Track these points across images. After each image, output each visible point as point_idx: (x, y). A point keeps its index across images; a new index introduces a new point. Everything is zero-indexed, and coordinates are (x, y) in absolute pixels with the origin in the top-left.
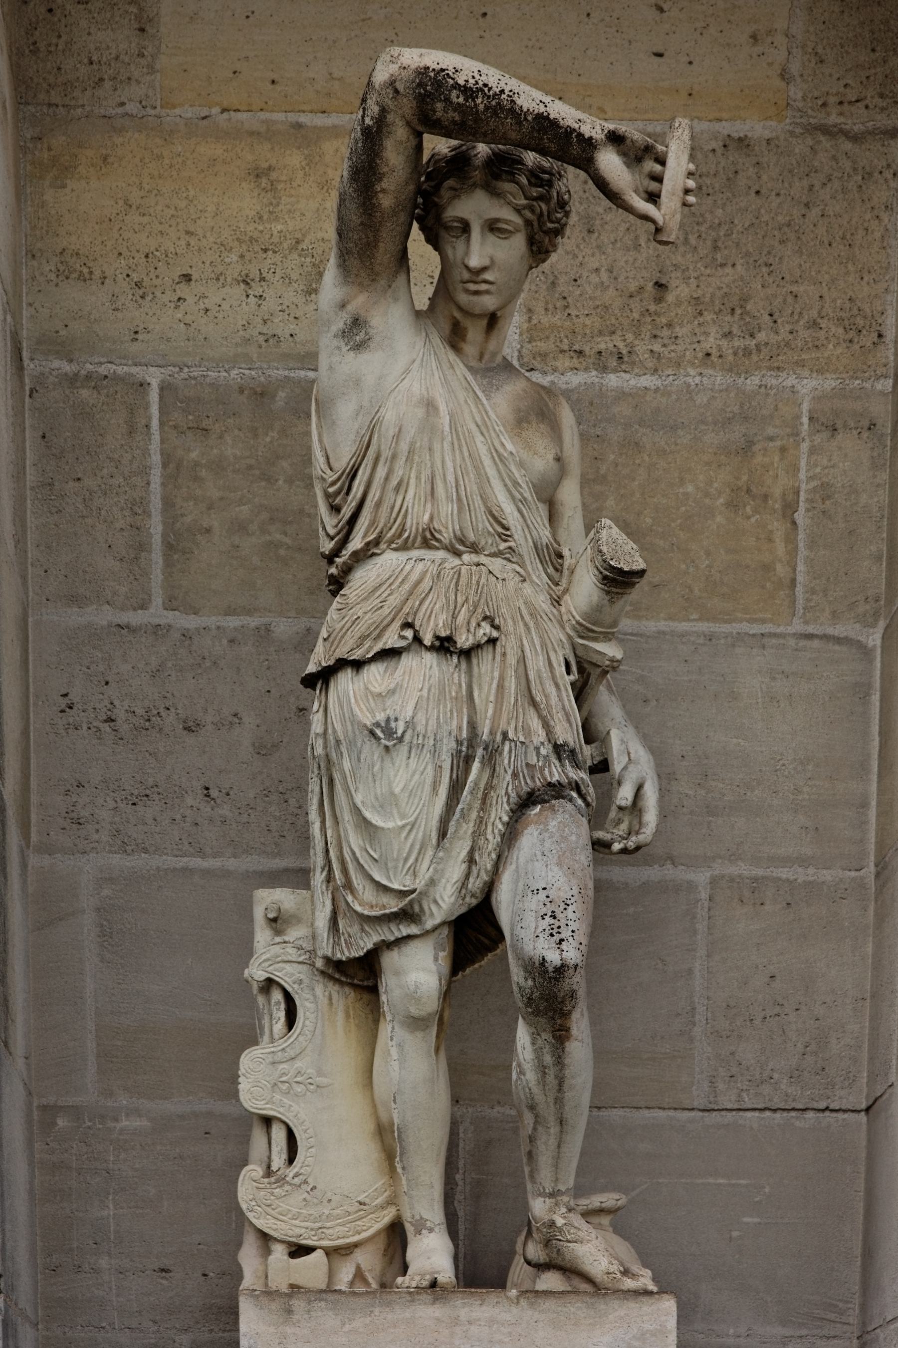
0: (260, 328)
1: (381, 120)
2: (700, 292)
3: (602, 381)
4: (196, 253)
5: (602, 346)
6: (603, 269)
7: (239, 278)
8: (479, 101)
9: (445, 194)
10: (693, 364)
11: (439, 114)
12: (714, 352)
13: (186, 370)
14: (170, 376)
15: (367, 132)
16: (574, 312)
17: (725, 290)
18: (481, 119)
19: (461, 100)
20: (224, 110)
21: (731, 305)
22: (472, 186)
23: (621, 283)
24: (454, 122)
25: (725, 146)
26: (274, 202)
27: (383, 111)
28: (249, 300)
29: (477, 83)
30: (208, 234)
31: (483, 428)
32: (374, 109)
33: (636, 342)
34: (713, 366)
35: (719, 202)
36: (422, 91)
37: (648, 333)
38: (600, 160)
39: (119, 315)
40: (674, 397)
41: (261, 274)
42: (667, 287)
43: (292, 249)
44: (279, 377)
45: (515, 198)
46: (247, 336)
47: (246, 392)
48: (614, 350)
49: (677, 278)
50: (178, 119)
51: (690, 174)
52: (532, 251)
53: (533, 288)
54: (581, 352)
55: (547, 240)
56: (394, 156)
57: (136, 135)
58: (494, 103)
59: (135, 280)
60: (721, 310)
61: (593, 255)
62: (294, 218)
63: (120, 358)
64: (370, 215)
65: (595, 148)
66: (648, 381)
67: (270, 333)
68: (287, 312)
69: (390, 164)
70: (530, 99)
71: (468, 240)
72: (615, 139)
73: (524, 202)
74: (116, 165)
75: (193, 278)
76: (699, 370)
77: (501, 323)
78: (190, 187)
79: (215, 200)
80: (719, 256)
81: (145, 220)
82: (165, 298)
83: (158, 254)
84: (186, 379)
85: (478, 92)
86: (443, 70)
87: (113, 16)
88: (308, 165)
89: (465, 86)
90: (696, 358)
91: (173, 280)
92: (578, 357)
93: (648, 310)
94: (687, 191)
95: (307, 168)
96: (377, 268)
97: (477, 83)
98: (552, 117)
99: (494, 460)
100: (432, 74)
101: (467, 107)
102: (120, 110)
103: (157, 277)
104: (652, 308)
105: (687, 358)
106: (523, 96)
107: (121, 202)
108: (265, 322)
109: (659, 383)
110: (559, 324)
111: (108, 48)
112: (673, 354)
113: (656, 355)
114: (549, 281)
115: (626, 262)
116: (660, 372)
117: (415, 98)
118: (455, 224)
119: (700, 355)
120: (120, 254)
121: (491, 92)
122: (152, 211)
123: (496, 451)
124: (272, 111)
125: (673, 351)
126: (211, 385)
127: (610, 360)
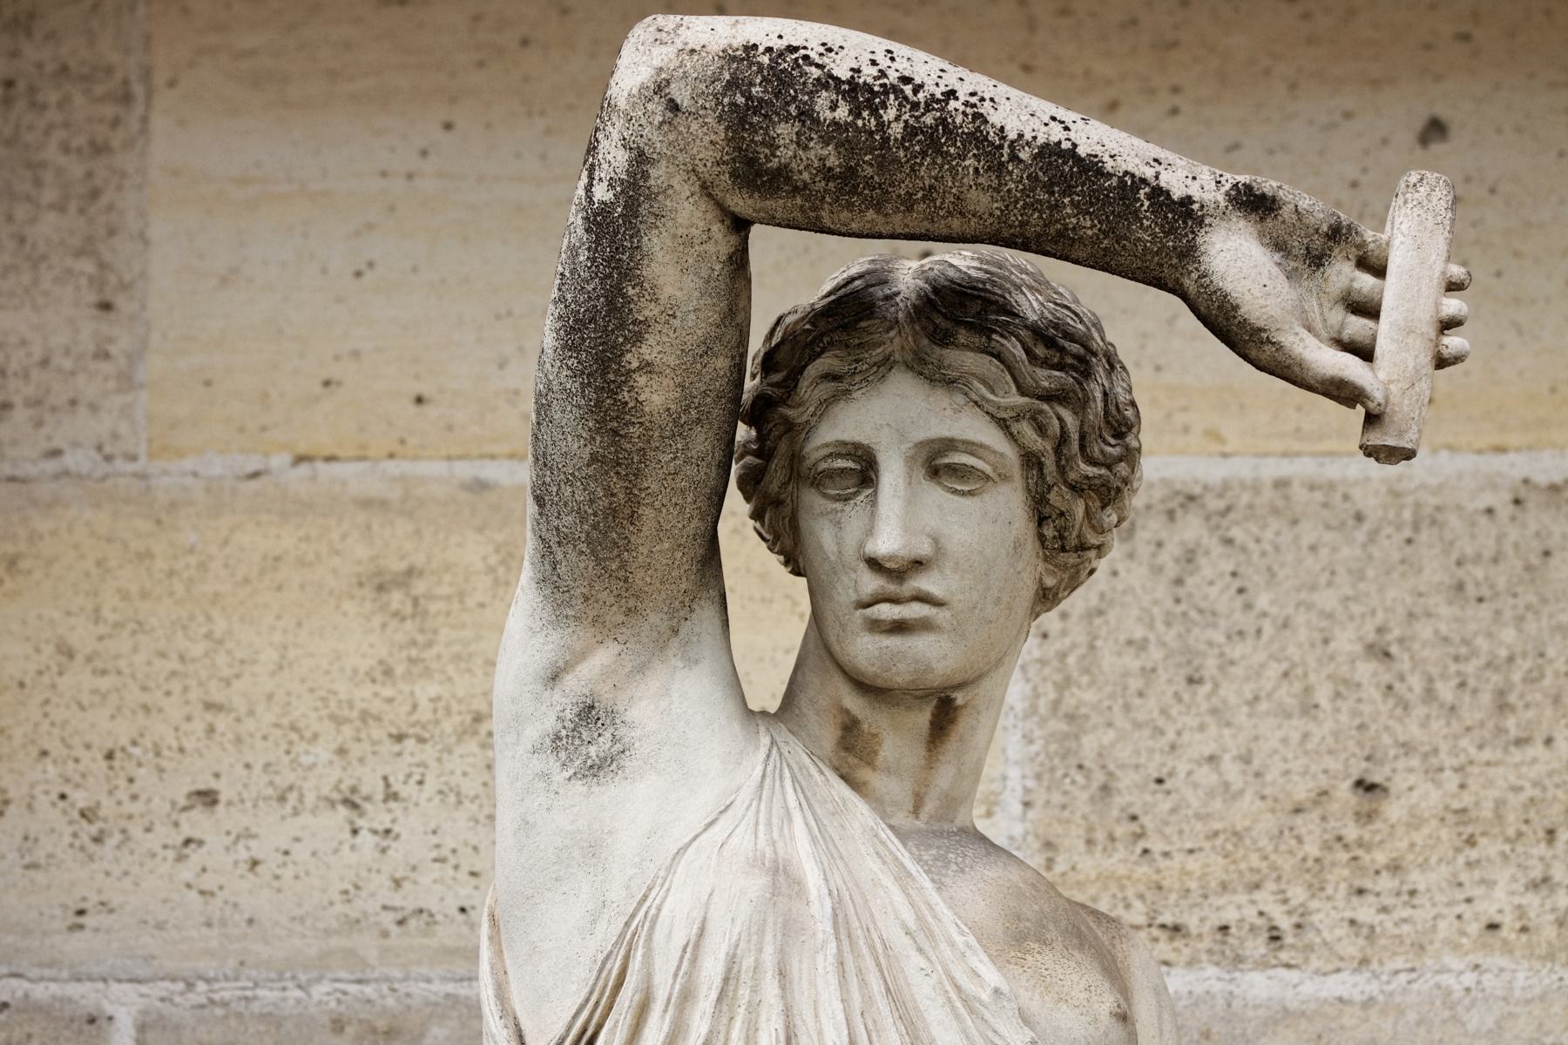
0: (388, 896)
1: (635, 188)
2: (1467, 800)
3: (1232, 987)
4: (229, 747)
5: (1230, 916)
6: (1227, 757)
7: (336, 796)
8: (890, 114)
9: (810, 389)
10: (1456, 947)
11: (785, 154)
12: (1508, 920)
13: (201, 986)
14: (162, 1000)
15: (599, 221)
16: (1157, 846)
17: (1530, 792)
18: (897, 160)
19: (842, 113)
20: (300, 459)
21: (1547, 823)
22: (878, 365)
23: (1273, 783)
24: (827, 173)
25: (1517, 502)
26: (421, 639)
27: (641, 159)
28: (358, 840)
29: (883, 74)
30: (260, 709)
31: (921, 938)
32: (614, 158)
33: (1314, 904)
34: (1507, 948)
35: (1508, 614)
36: (740, 100)
37: (1343, 886)
38: (1213, 251)
39: (39, 877)
40: (1412, 1016)
41: (388, 785)
42: (1385, 790)
43: (462, 734)
44: (433, 998)
45: (993, 392)
46: (354, 915)
47: (349, 1030)
48: (1260, 922)
49: (1411, 770)
50: (189, 480)
51: (1453, 287)
52: (1042, 538)
53: (1057, 798)
54: (1176, 929)
55: (1079, 509)
56: (674, 273)
57: (89, 514)
58: (928, 120)
59: (81, 804)
60: (1520, 835)
61: (1202, 728)
62: (469, 670)
63: (41, 965)
64: (615, 432)
65: (1200, 222)
66: (1346, 984)
67: (410, 905)
68: (452, 860)
69: (663, 298)
70: (1021, 113)
71: (873, 502)
72: (1253, 204)
73: (1017, 400)
74: (38, 575)
75: (223, 798)
76: (1473, 958)
77: (963, 723)
78: (216, 614)
79: (277, 637)
80: (1511, 722)
81: (105, 683)
82: (153, 842)
83: (137, 751)
84: (202, 1006)
85: (886, 93)
86: (792, 49)
87: (36, 282)
88: (503, 562)
89: (851, 81)
90: (1463, 933)
91: (173, 803)
92: (1171, 939)
93: (1339, 839)
94: (1448, 325)
95: (501, 570)
96: (639, 578)
97: (883, 74)
98: (1082, 151)
99: (953, 1008)
100: (765, 60)
101: (858, 130)
102: (51, 466)
103: (134, 797)
104: (1352, 832)
105: (1441, 935)
106: (1004, 107)
107: (48, 650)
108: (397, 883)
109: (1373, 988)
110: (1122, 870)
111: (23, 343)
112: (1406, 928)
113: (1365, 931)
114: (1095, 785)
115: (1285, 741)
116: (1375, 965)
117: (720, 119)
118: (841, 463)
119: (1474, 928)
120: (44, 753)
121: (921, 95)
122: (122, 664)
123: (958, 988)
124: (416, 458)
125: (1405, 921)
126: (264, 1017)
127: (1249, 944)
